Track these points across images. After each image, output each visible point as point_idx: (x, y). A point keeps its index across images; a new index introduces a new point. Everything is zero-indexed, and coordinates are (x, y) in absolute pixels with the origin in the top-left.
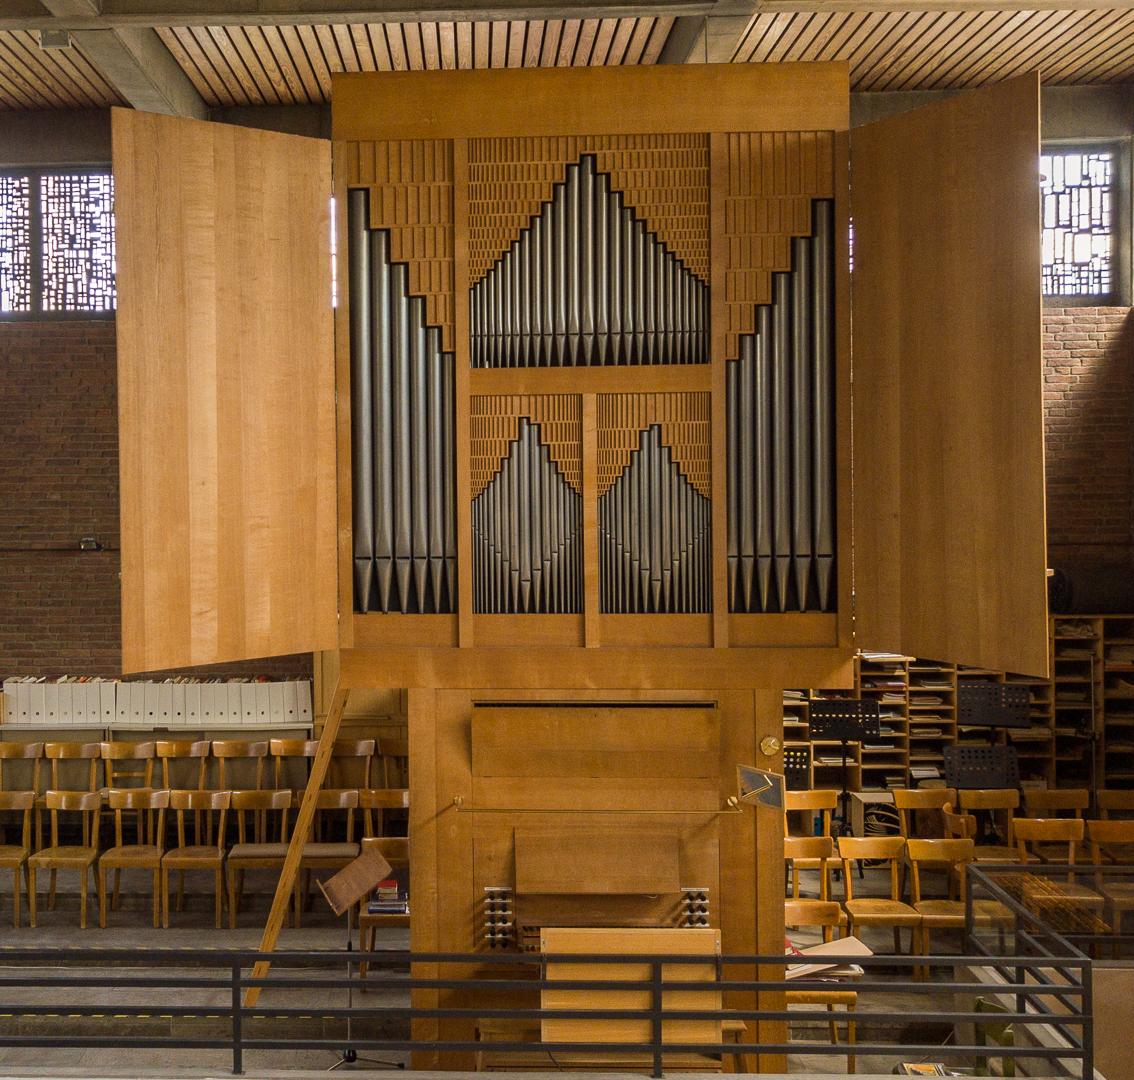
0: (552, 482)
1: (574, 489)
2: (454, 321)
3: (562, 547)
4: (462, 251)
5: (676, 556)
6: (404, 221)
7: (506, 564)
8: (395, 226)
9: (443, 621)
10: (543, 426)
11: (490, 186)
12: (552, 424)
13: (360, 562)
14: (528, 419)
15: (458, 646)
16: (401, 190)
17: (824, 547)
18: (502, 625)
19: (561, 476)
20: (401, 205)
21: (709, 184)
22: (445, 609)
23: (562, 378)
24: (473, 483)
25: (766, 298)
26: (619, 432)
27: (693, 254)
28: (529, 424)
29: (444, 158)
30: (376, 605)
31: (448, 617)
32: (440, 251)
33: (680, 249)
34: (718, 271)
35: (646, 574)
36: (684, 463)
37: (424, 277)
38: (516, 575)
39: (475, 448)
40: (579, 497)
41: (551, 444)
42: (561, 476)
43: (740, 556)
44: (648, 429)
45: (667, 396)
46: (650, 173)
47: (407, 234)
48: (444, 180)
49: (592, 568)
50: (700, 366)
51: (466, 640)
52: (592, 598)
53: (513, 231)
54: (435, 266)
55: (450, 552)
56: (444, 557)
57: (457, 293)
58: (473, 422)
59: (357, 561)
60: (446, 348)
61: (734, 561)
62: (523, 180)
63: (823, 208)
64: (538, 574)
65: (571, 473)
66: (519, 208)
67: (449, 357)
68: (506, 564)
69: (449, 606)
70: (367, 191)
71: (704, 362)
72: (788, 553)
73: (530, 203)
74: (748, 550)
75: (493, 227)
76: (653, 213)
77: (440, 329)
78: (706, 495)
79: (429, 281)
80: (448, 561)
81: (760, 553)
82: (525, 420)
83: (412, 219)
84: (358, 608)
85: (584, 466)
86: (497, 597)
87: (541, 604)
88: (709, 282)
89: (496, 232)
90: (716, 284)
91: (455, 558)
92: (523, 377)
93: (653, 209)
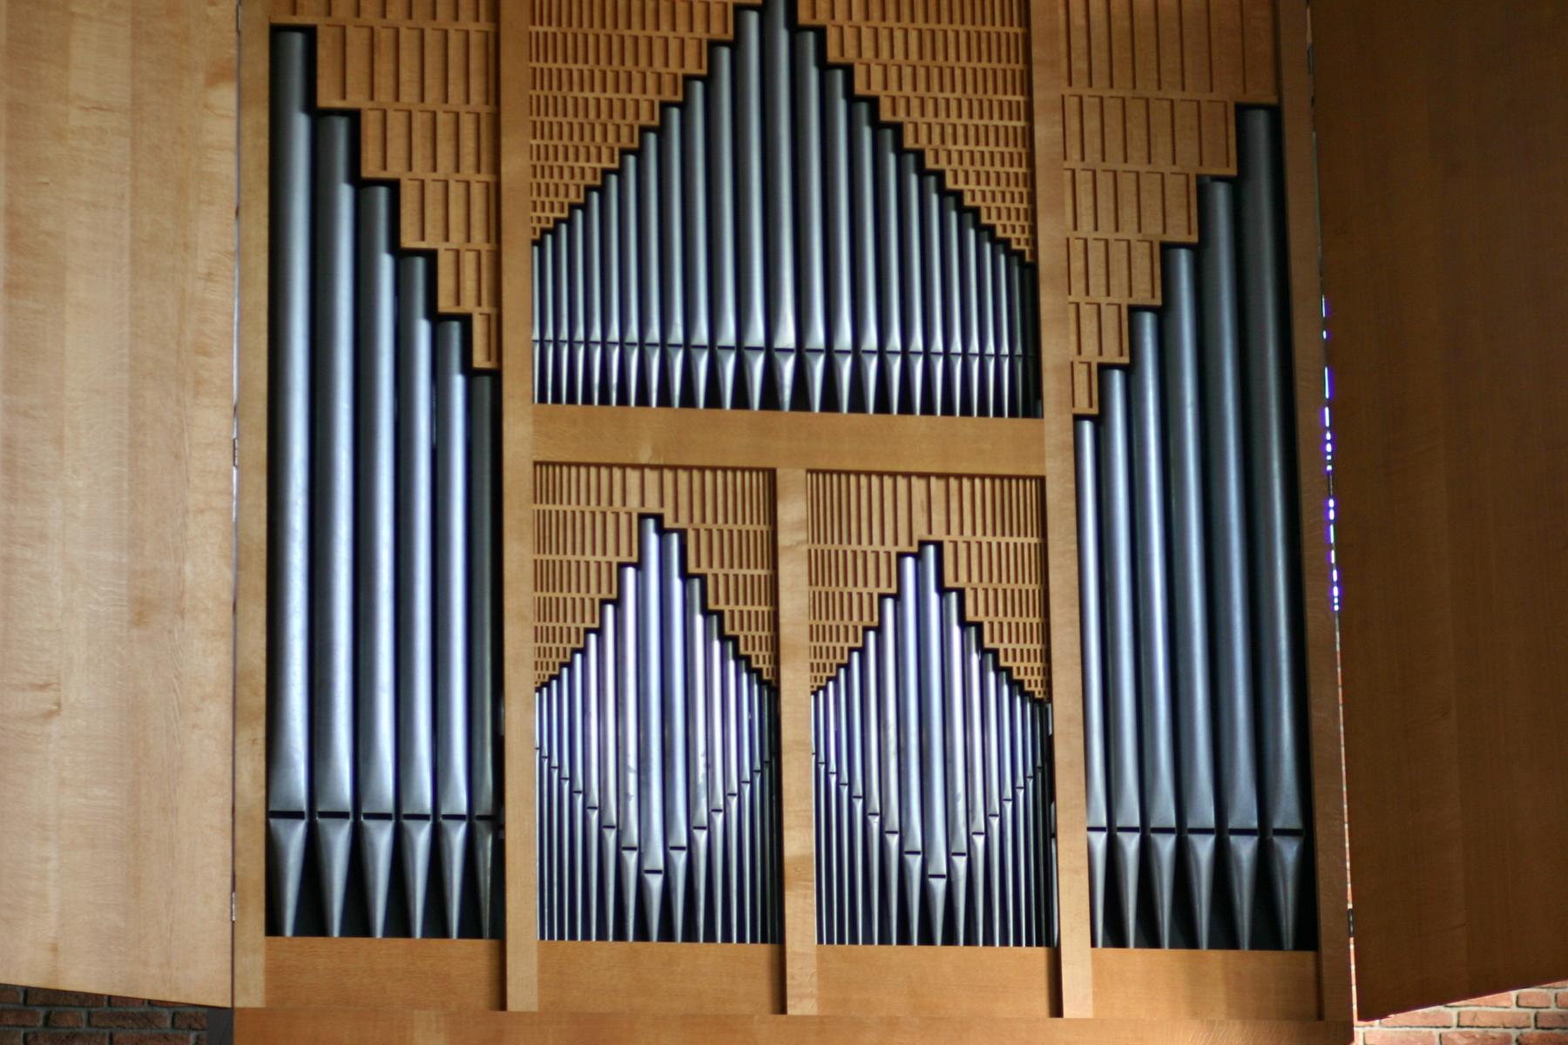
0: (709, 656)
1: (759, 671)
2: (497, 301)
3: (995, 822)
4: (515, 165)
5: (979, 824)
6: (415, 98)
7: (611, 836)
8: (370, 104)
9: (465, 956)
10: (691, 535)
11: (575, 36)
12: (710, 532)
13: (279, 825)
14: (659, 518)
15: (502, 1004)
16: (385, 36)
17: (1286, 812)
18: (604, 962)
19: (1016, 686)
20: (384, 67)
21: (1028, 60)
22: (470, 929)
23: (736, 436)
24: (541, 652)
25: (1181, 230)
26: (855, 553)
27: (999, 196)
28: (662, 532)
29: (700, 54)
30: (313, 921)
31: (480, 948)
32: (468, 159)
33: (972, 186)
34: (1050, 232)
35: (915, 863)
36: (992, 624)
37: (434, 213)
38: (631, 859)
39: (543, 576)
40: (771, 690)
41: (710, 572)
42: (1016, 686)
43: (1112, 830)
44: (915, 549)
45: (953, 483)
46: (876, 30)
47: (397, 123)
48: (477, 19)
49: (799, 842)
50: (1021, 422)
51: (523, 992)
52: (800, 909)
53: (625, 131)
54: (456, 191)
55: (485, 803)
56: (470, 818)
57: (504, 248)
58: (542, 519)
59: (272, 821)
60: (480, 360)
61: (1100, 840)
62: (644, 27)
63: (1260, 125)
64: (680, 859)
65: (753, 640)
66: (637, 84)
67: (487, 387)
68: (611, 836)
69: (485, 918)
70: (310, 33)
71: (1027, 415)
72: (1255, 824)
73: (659, 76)
74: (1130, 813)
75: (581, 117)
76: (915, 114)
77: (466, 321)
78: (1038, 692)
79: (441, 222)
80: (481, 826)
81: (1234, 822)
82: (651, 523)
83: (409, 94)
84: (273, 926)
85: (783, 620)
86: (594, 904)
87: (685, 919)
88: (1035, 253)
89: (587, 129)
90: (1048, 260)
91: (496, 820)
92: (647, 431)
93: (915, 103)
